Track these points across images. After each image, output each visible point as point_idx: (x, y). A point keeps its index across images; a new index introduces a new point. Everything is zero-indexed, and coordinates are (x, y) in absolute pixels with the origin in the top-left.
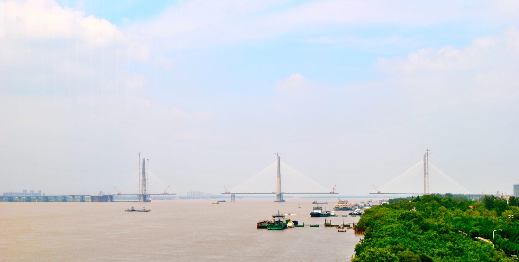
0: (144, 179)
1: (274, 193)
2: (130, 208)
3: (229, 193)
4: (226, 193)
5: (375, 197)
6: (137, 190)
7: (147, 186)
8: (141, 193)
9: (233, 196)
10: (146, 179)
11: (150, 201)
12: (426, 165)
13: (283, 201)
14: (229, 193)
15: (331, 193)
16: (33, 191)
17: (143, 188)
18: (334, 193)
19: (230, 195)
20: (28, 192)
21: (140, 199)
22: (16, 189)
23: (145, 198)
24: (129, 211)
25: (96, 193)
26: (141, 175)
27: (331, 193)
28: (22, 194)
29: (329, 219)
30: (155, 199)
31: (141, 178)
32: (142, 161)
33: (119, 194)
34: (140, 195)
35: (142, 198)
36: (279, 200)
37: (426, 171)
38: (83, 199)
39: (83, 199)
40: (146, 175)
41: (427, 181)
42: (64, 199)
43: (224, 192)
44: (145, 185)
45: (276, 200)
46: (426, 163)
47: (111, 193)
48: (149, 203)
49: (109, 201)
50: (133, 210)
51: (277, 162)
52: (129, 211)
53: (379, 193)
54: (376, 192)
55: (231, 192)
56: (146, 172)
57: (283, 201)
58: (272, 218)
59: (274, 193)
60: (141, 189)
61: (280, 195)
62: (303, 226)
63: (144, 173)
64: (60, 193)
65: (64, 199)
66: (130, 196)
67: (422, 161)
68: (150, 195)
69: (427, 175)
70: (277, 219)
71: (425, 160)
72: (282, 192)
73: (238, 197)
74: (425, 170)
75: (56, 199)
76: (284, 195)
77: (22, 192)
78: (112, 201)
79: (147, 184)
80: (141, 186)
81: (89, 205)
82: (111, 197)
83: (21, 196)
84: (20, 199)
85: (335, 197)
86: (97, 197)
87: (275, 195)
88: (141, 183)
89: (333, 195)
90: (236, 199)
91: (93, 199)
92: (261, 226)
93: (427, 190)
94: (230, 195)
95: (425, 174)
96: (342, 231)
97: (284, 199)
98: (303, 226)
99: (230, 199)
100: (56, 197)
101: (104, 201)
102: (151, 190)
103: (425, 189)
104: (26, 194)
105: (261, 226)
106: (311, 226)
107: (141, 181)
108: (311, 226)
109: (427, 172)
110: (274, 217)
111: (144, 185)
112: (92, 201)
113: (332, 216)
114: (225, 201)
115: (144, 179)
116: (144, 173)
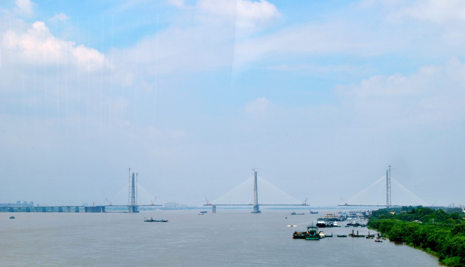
0: (133, 192)
1: (251, 205)
2: (149, 219)
3: (210, 205)
4: (208, 205)
5: (344, 209)
6: (126, 201)
7: (136, 198)
8: (130, 204)
9: (214, 207)
10: (135, 191)
11: (139, 212)
12: (389, 180)
13: (259, 212)
14: (210, 205)
15: (302, 205)
16: (26, 202)
17: (132, 200)
18: (305, 205)
19: (211, 207)
20: (28, 203)
21: (129, 209)
22: (12, 200)
23: (134, 209)
24: (148, 221)
25: (90, 205)
26: (131, 188)
27: (302, 205)
28: (17, 205)
29: (356, 229)
30: (141, 209)
31: (131, 191)
32: (131, 176)
33: (111, 205)
34: (130, 206)
35: (132, 209)
36: (256, 211)
37: (389, 185)
38: (77, 210)
39: (77, 210)
40: (135, 188)
41: (389, 194)
42: (60, 210)
43: (206, 204)
44: (134, 197)
45: (253, 211)
46: (389, 178)
47: (103, 205)
48: (138, 213)
49: (102, 211)
50: (152, 221)
51: (254, 176)
52: (148, 221)
53: (346, 205)
54: (344, 204)
55: (212, 204)
56: (135, 186)
57: (259, 212)
58: (306, 229)
59: (251, 205)
60: (131, 200)
61: (257, 207)
62: (332, 236)
63: (133, 186)
64: (42, 204)
65: (60, 210)
66: (229, 206)
67: (385, 176)
68: (138, 206)
69: (389, 189)
70: (311, 229)
71: (387, 175)
72: (259, 203)
73: (218, 208)
74: (387, 184)
75: (52, 209)
76: (260, 206)
77: (16, 203)
78: (104, 212)
79: (136, 196)
80: (130, 198)
81: (82, 215)
82: (103, 208)
83: (21, 206)
84: (20, 210)
85: (307, 209)
86: (90, 208)
87: (253, 206)
88: (131, 196)
89: (305, 206)
90: (216, 209)
91: (87, 209)
92: (296, 236)
93: (389, 202)
94: (211, 207)
95: (387, 188)
96: (379, 241)
97: (260, 210)
98: (332, 236)
99: (212, 210)
100: (52, 208)
101: (97, 212)
102: (139, 202)
103: (388, 201)
104: (20, 205)
105: (296, 236)
106: (338, 236)
107: (131, 194)
108: (338, 236)
109: (389, 186)
110: (309, 228)
111: (133, 197)
112: (86, 211)
113: (335, 226)
114: (317, 213)
115: (133, 192)
116: (133, 186)
